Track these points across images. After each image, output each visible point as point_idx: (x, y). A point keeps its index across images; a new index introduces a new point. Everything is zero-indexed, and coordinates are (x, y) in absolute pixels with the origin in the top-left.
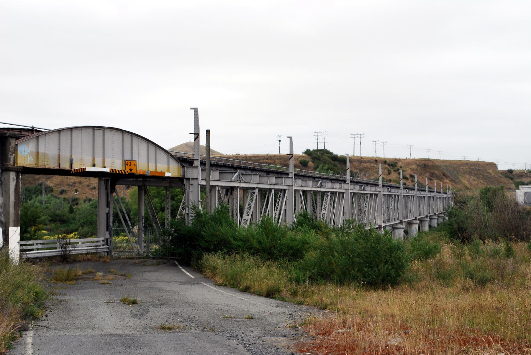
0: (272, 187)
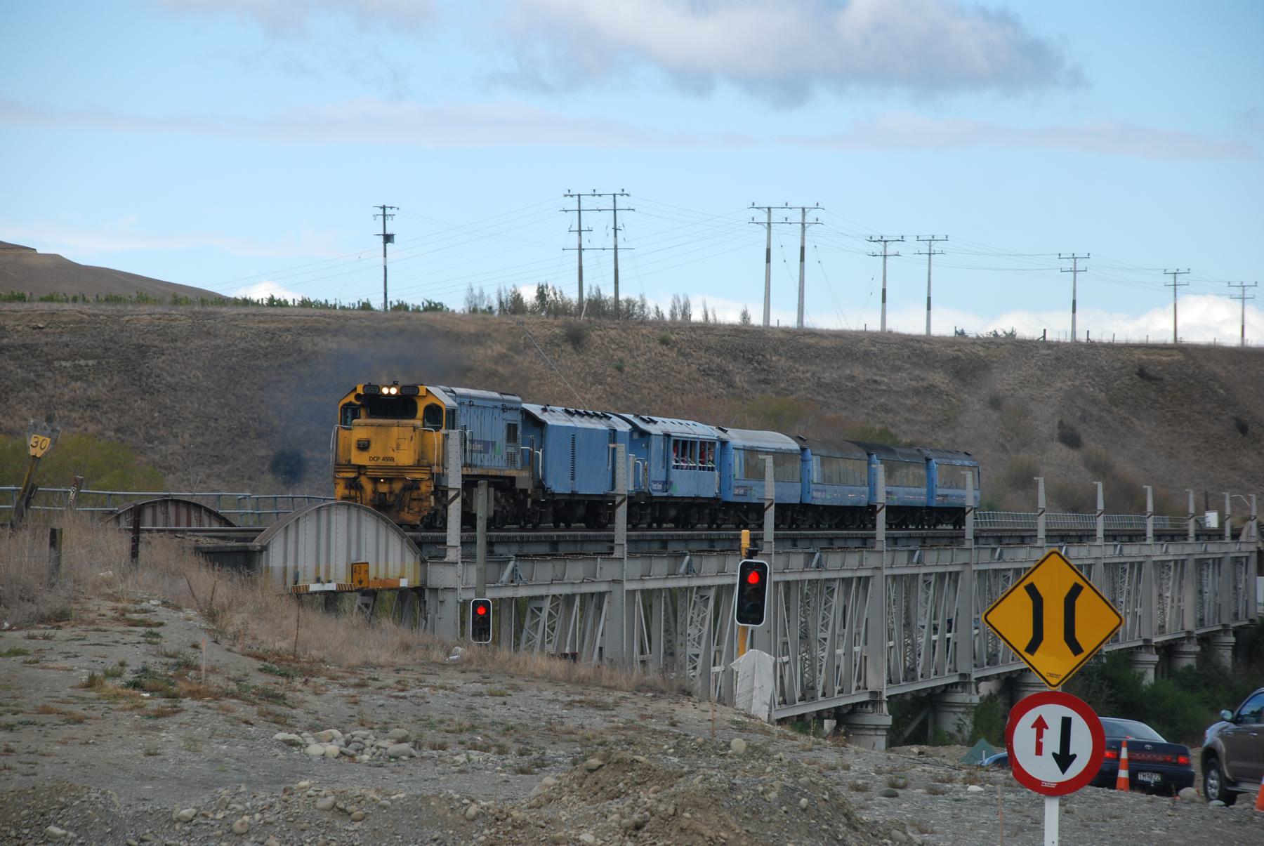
0: (576, 590)
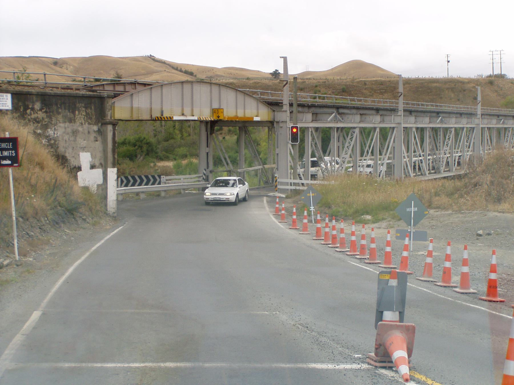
0: (376, 126)
